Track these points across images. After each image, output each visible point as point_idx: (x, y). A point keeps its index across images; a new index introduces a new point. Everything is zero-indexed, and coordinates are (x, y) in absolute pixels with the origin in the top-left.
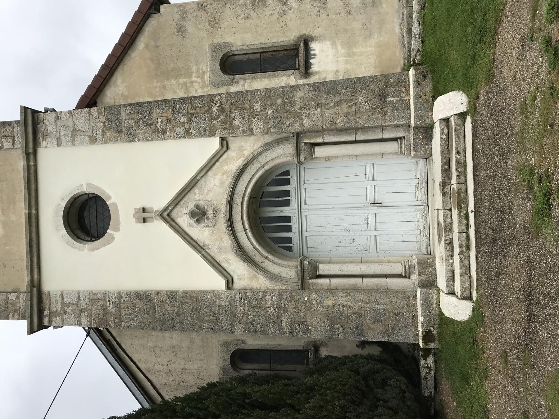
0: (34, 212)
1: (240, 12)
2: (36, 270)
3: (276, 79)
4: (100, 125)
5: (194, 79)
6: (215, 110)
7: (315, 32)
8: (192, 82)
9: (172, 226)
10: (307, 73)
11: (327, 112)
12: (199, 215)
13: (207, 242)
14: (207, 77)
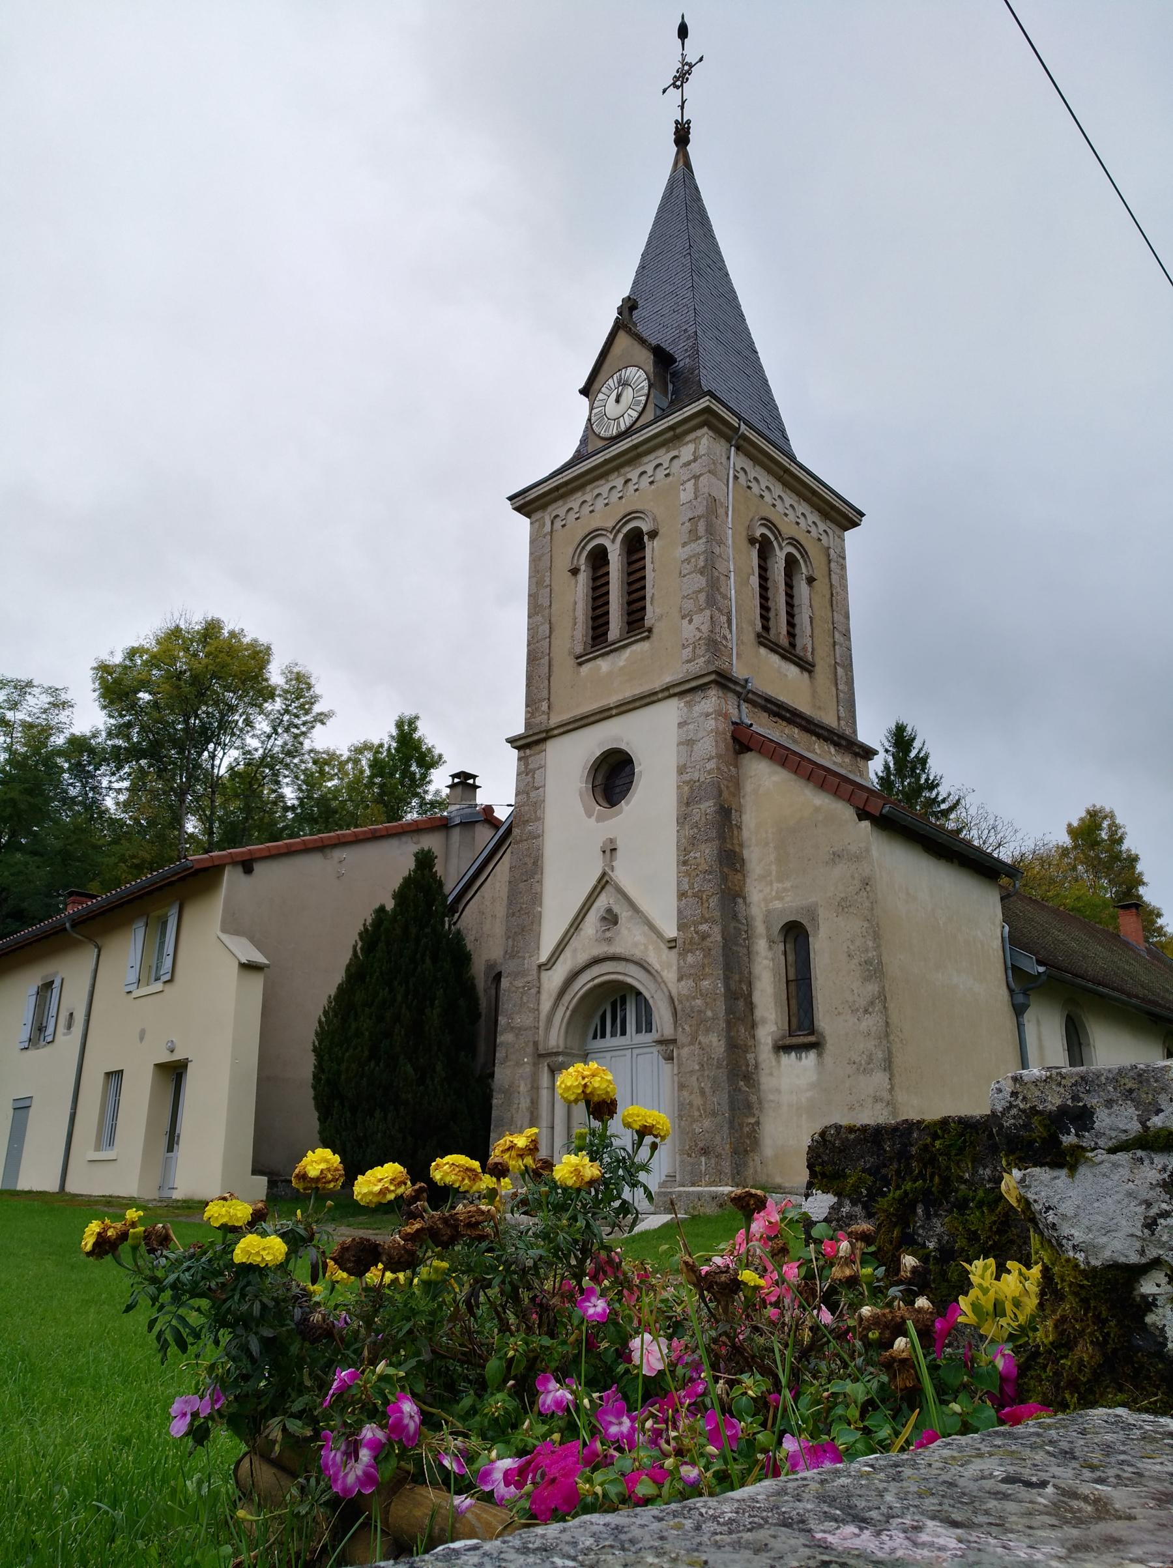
0: (614, 712)
1: (857, 943)
2: (561, 730)
3: (772, 1005)
4: (696, 776)
5: (775, 886)
6: (704, 927)
7: (828, 1058)
8: (771, 884)
9: (595, 888)
10: (782, 1048)
11: (694, 1078)
12: (611, 919)
13: (582, 933)
14: (778, 905)
